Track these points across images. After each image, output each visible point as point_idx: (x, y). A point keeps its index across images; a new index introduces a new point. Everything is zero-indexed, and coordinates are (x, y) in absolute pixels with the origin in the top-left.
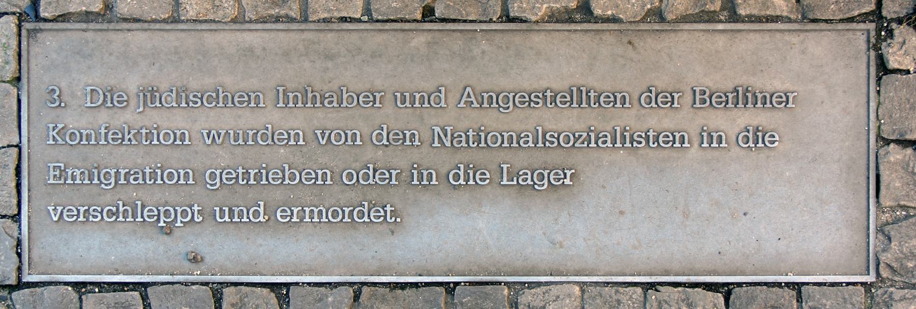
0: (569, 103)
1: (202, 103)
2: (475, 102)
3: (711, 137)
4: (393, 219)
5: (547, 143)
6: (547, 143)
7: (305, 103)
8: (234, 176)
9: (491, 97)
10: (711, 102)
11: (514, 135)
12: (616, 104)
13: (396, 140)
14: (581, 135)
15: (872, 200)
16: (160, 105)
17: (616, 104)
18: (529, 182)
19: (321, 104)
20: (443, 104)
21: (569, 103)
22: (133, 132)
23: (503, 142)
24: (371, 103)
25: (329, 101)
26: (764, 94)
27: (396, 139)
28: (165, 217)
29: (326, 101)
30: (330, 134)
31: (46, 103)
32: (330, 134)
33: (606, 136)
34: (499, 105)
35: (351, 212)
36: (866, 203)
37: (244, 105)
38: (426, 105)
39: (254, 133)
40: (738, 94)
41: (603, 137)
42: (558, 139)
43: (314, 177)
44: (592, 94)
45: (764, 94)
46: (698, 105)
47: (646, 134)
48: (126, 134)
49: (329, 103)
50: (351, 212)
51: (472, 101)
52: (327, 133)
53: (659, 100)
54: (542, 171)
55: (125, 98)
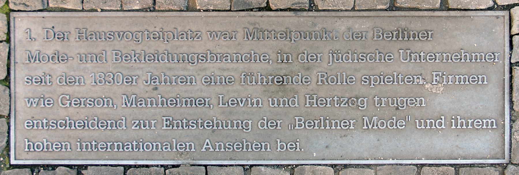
0: (285, 38)
1: (94, 105)
2: (211, 148)
3: (331, 123)
5: (195, 123)
6: (195, 123)
7: (403, 38)
8: (32, 124)
9: (337, 123)
10: (383, 36)
12: (495, 60)
16: (478, 76)
17: (495, 60)
19: (222, 127)
20: (296, 105)
21: (285, 38)
24: (260, 149)
29: (125, 148)
31: (330, 66)
34: (189, 61)
35: (473, 123)
36: (126, 122)
37: (458, 61)
38: (287, 106)
39: (472, 122)
40: (321, 121)
43: (83, 124)
46: (375, 39)
47: (197, 121)
49: (182, 38)
50: (473, 123)
51: (209, 148)
53: (269, 124)
55: (52, 102)
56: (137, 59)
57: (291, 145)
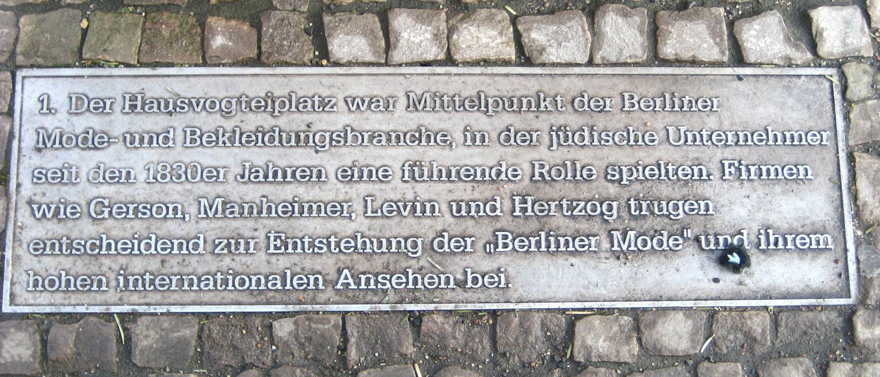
4: (311, 250)
5: (379, 284)
11: (262, 277)
13: (79, 103)
14: (330, 101)
15: (837, 96)
18: (665, 212)
22: (227, 135)
23: (167, 213)
25: (206, 284)
26: (398, 239)
27: (76, 105)
28: (662, 240)
30: (205, 102)
32: (205, 102)
33: (276, 279)
41: (273, 280)
42: (151, 210)
44: (670, 167)
45: (398, 239)
47: (327, 240)
48: (220, 136)
52: (202, 101)
54: (415, 239)
56: (227, 141)
57: (95, 103)
